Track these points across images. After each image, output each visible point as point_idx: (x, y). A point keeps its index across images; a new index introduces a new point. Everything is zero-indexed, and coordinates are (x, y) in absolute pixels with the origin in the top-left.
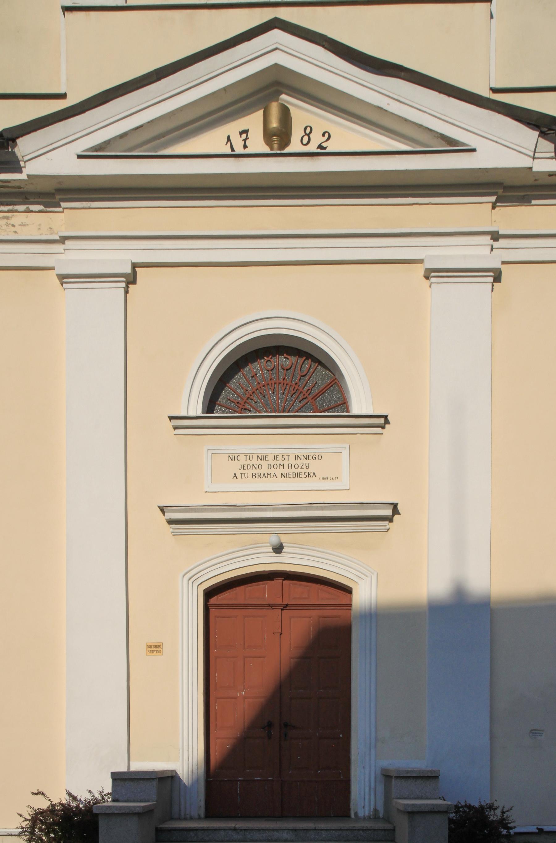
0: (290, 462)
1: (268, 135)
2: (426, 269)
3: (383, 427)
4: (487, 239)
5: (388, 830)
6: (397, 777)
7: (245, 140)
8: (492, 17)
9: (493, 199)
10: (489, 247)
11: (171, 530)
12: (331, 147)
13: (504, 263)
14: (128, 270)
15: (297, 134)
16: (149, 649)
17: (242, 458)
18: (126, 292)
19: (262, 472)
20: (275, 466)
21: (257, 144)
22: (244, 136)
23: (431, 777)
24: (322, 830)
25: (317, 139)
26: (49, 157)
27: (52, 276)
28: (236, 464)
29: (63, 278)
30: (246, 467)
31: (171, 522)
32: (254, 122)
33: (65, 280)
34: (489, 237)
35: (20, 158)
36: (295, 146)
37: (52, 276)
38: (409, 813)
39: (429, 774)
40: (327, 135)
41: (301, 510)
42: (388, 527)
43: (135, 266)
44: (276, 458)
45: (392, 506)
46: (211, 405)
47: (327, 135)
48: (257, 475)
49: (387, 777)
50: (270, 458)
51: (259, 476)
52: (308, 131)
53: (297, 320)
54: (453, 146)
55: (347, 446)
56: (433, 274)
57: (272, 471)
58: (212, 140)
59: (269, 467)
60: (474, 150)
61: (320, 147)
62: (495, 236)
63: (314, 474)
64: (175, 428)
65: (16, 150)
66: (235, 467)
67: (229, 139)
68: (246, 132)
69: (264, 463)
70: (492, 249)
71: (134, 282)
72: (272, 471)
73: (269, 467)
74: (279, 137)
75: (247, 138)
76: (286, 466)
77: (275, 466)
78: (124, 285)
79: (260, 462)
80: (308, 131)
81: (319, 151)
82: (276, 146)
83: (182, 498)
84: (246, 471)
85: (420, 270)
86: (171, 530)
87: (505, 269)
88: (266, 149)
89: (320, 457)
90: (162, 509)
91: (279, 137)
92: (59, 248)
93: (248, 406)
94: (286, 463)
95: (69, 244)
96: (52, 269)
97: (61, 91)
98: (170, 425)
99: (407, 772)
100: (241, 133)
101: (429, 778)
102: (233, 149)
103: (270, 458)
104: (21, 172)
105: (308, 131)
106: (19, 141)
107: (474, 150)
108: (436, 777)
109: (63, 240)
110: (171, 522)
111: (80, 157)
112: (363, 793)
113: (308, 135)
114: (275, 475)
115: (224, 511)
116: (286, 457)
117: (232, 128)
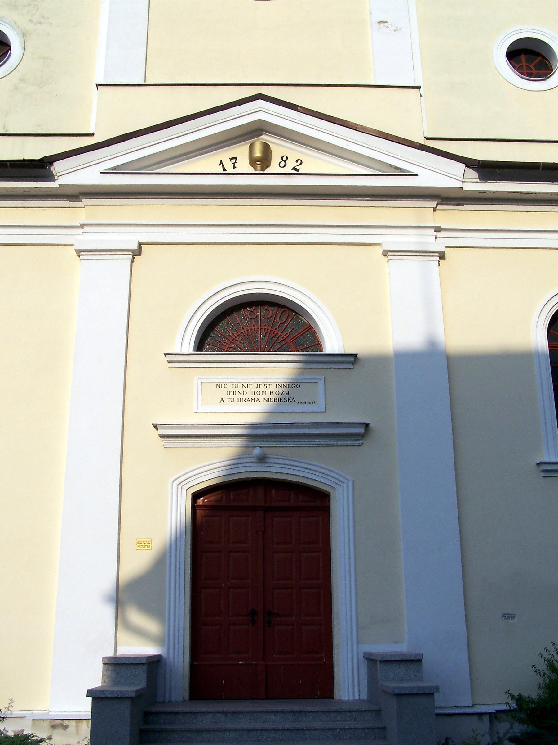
0: (271, 389)
1: (253, 162)
2: (384, 250)
3: (353, 363)
4: (432, 231)
5: (374, 711)
6: (381, 661)
7: (234, 163)
8: (421, 96)
9: (434, 204)
10: (434, 237)
11: (163, 443)
12: (302, 170)
13: (446, 247)
14: (135, 247)
15: (275, 159)
16: (139, 544)
17: (229, 387)
18: (132, 261)
19: (246, 397)
20: (258, 393)
21: (244, 165)
22: (233, 161)
23: (416, 661)
24: (310, 712)
25: (291, 163)
26: (67, 175)
27: (72, 250)
28: (223, 391)
29: (79, 252)
30: (232, 393)
31: (162, 436)
32: (241, 152)
33: (82, 253)
34: (433, 230)
35: (55, 174)
36: (274, 168)
37: (72, 250)
38: (396, 695)
39: (413, 658)
40: (299, 162)
41: (282, 428)
42: (361, 442)
43: (140, 244)
44: (259, 386)
45: (364, 426)
46: (201, 344)
47: (299, 162)
48: (242, 400)
49: (372, 661)
50: (254, 386)
51: (244, 400)
52: (284, 158)
53: (27, 226)
54: (399, 172)
55: (323, 378)
56: (389, 253)
57: (256, 396)
58: (209, 163)
59: (253, 393)
60: (417, 175)
61: (294, 169)
62: (438, 229)
63: (293, 399)
64: (169, 362)
65: (52, 168)
66: (222, 393)
67: (221, 162)
68: (236, 158)
69: (249, 390)
70: (436, 238)
71: (139, 254)
72: (256, 396)
73: (253, 393)
74: (262, 162)
75: (236, 162)
76: (268, 393)
77: (258, 393)
78: (131, 257)
79: (244, 389)
80: (284, 158)
81: (294, 172)
82: (259, 168)
83: (173, 417)
84: (232, 397)
85: (379, 251)
86: (163, 443)
87: (447, 251)
88: (252, 170)
89: (298, 386)
90: (155, 427)
91: (262, 162)
92: (80, 231)
93: (233, 346)
94: (268, 390)
95: (86, 229)
96: (73, 245)
97: (91, 132)
98: (165, 359)
99: (391, 656)
100: (231, 159)
101: (412, 661)
102: (224, 170)
103: (254, 386)
104: (54, 180)
105: (284, 159)
106: (54, 164)
107: (417, 175)
108: (420, 661)
109: (82, 226)
110: (162, 436)
111: (102, 173)
112: (349, 682)
113: (285, 161)
114: (258, 400)
115: (213, 428)
116: (268, 386)
117: (225, 155)
